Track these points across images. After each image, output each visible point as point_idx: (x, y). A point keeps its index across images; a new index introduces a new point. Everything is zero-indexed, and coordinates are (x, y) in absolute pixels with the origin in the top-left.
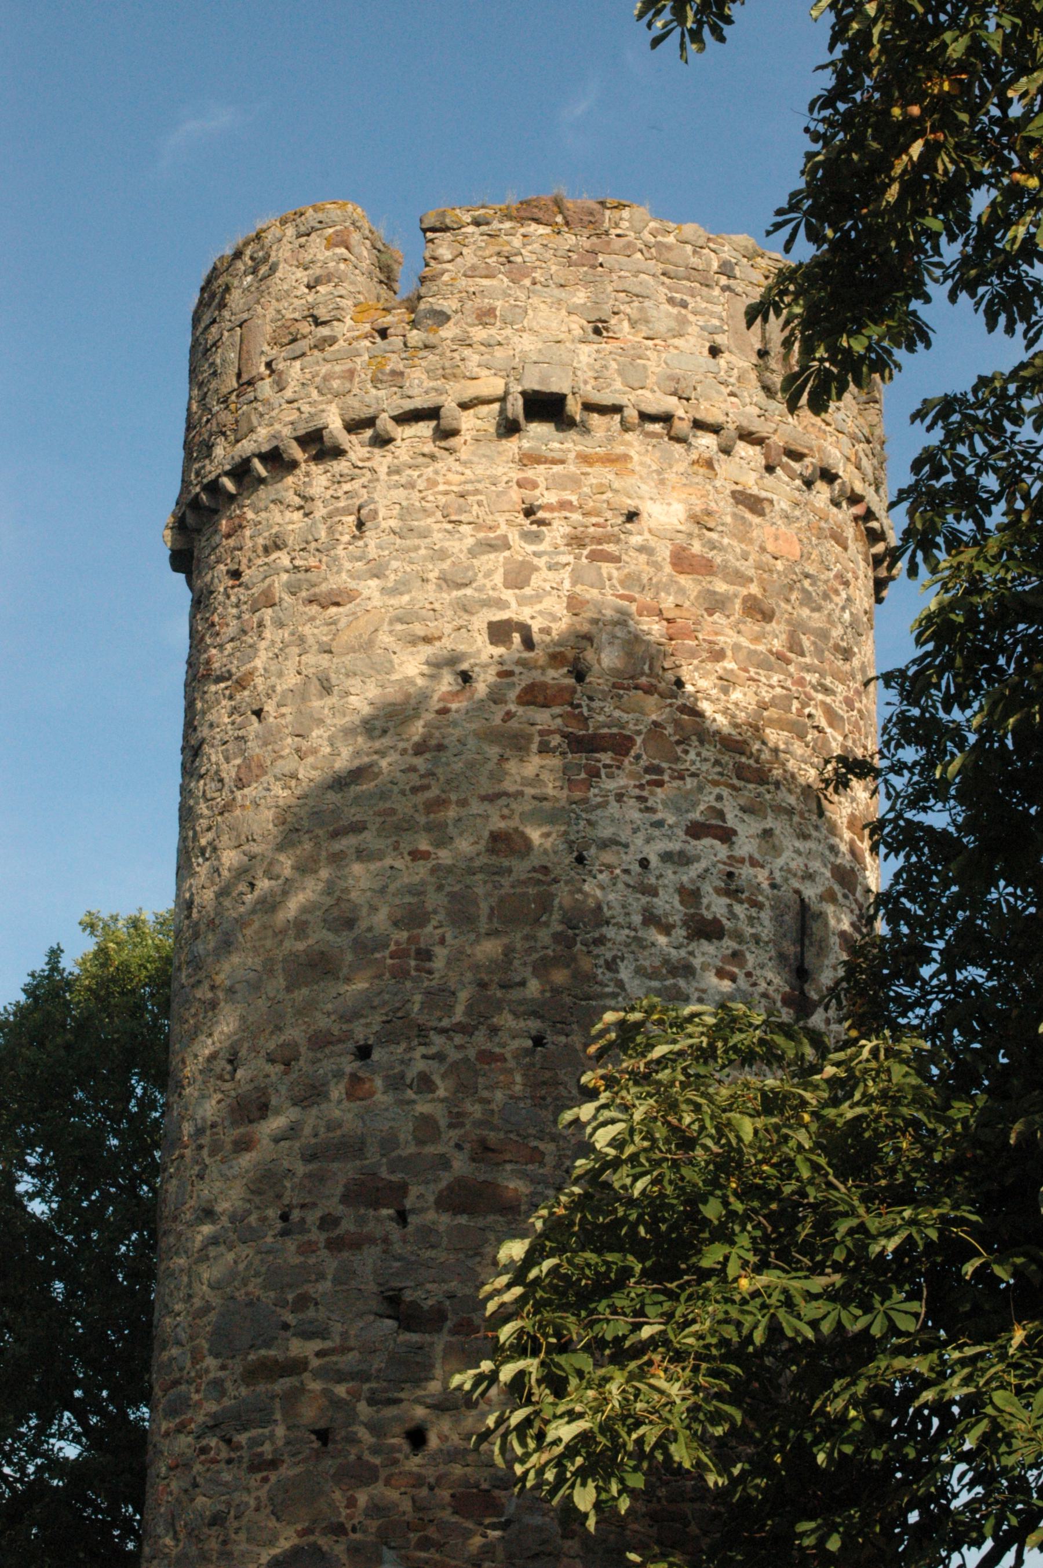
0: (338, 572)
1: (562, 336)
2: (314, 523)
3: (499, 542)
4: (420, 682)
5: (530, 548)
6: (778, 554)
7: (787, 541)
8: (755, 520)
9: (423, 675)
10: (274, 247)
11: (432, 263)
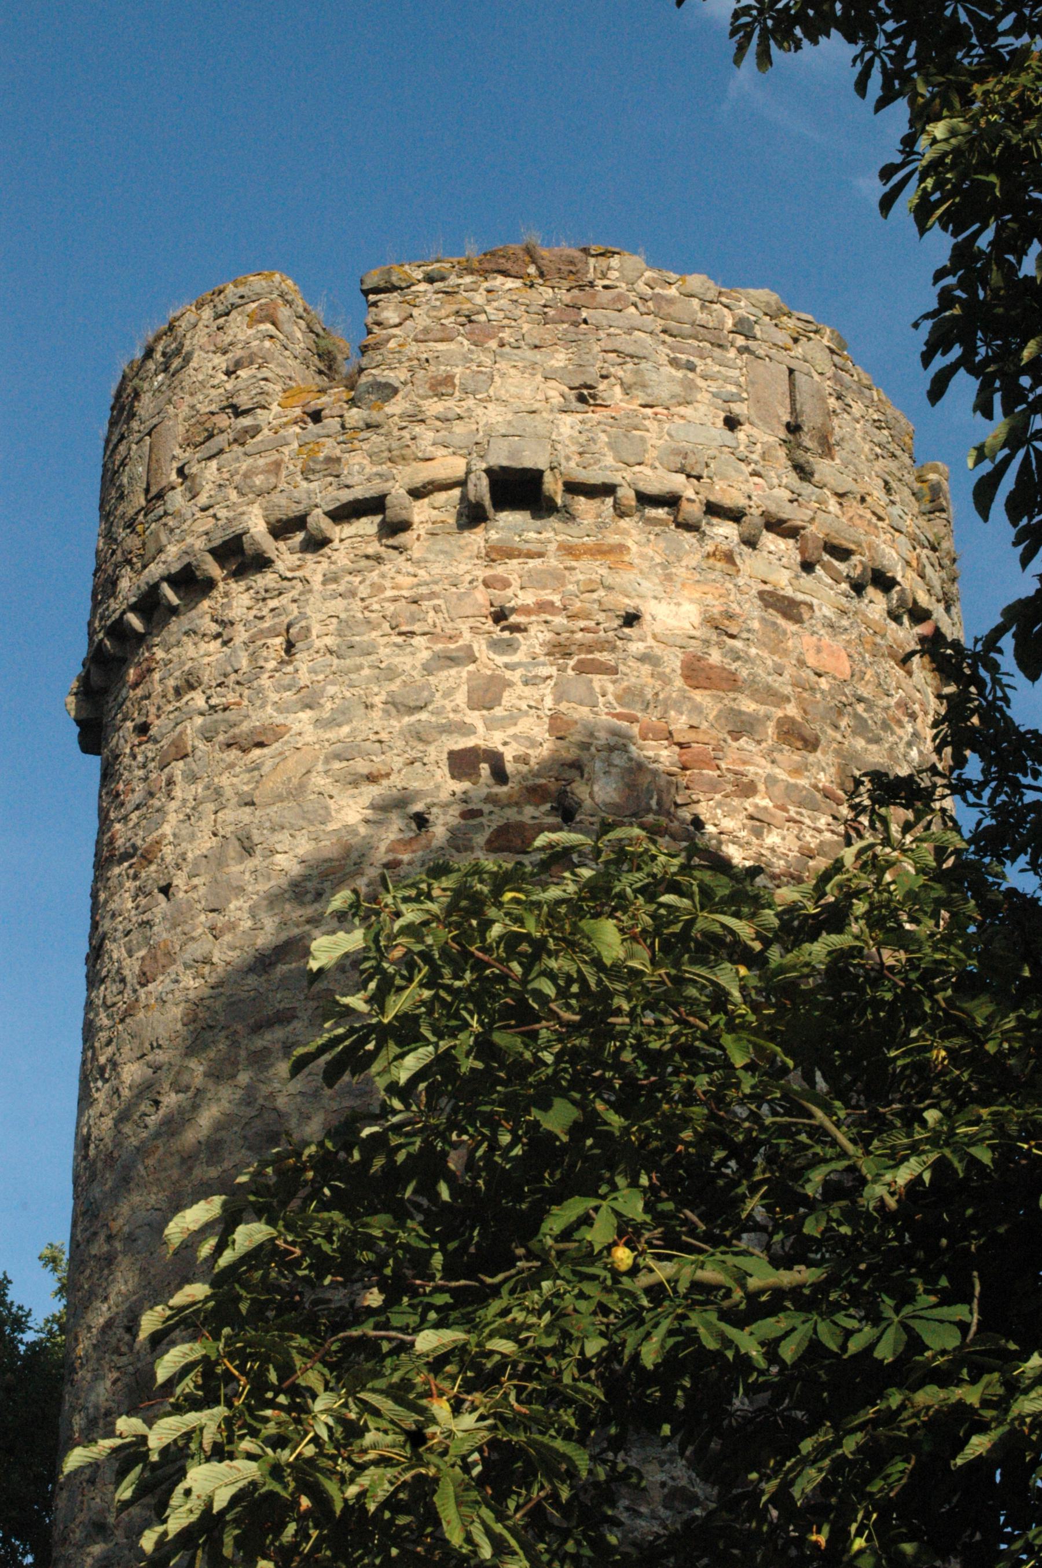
0: (263, 706)
1: (537, 406)
2: (234, 651)
3: (461, 654)
4: (363, 830)
5: (501, 660)
6: (821, 670)
7: (832, 654)
8: (791, 627)
9: (367, 821)
10: (188, 336)
11: (376, 329)
